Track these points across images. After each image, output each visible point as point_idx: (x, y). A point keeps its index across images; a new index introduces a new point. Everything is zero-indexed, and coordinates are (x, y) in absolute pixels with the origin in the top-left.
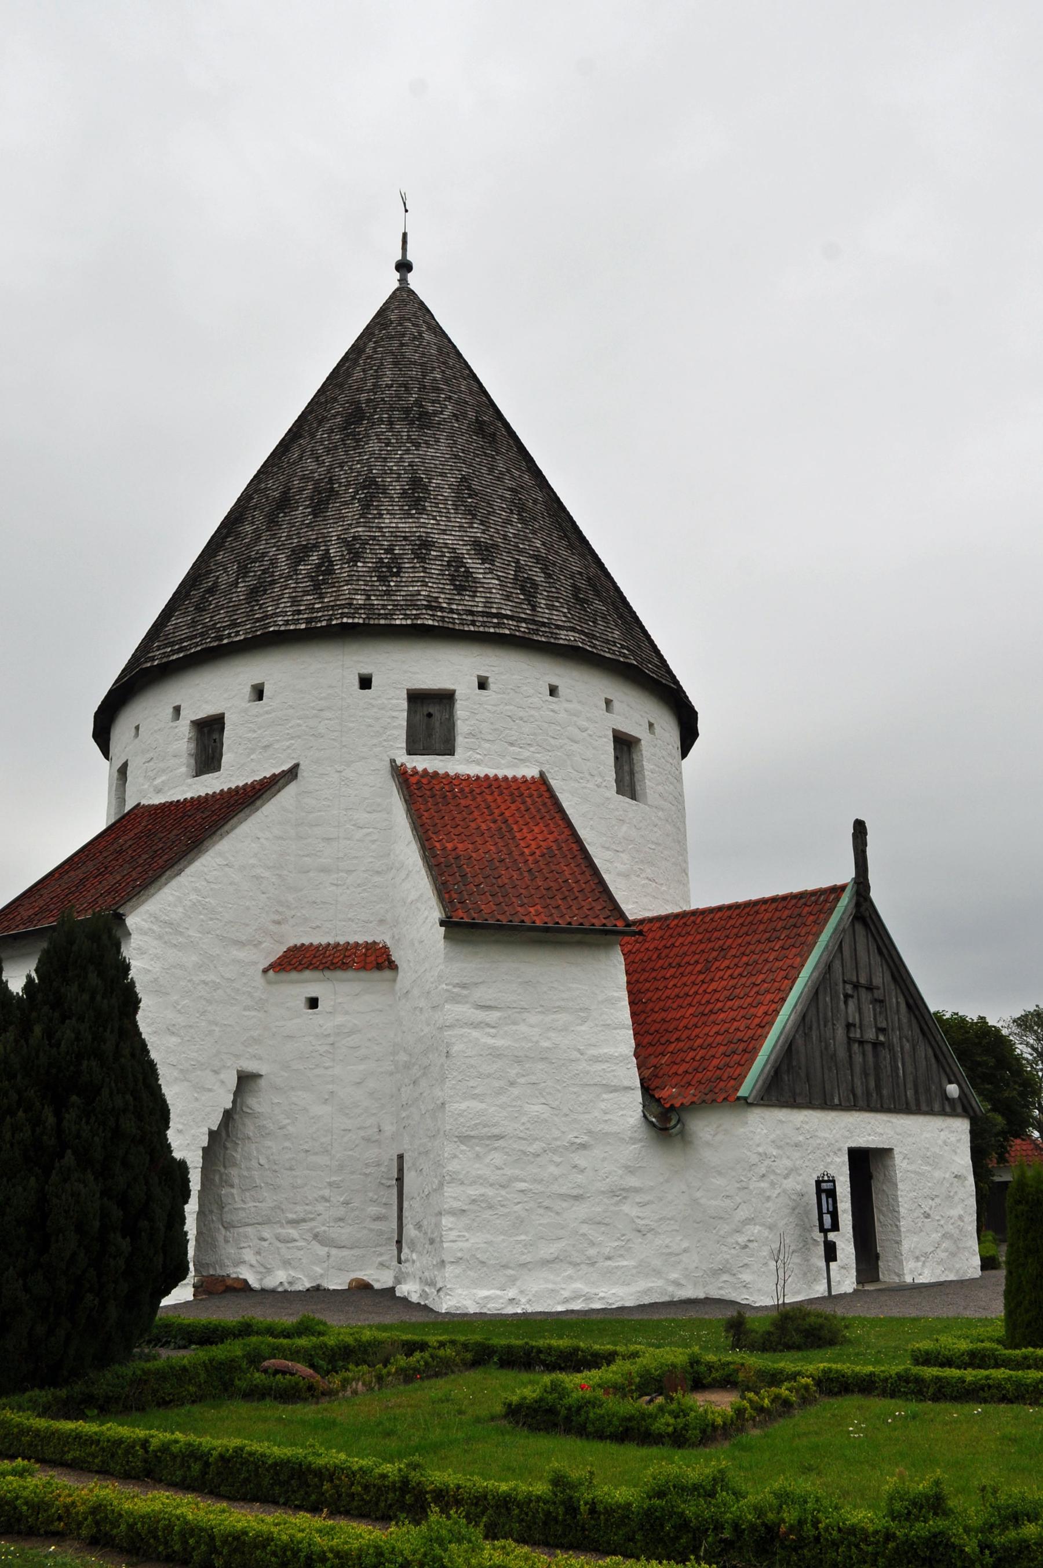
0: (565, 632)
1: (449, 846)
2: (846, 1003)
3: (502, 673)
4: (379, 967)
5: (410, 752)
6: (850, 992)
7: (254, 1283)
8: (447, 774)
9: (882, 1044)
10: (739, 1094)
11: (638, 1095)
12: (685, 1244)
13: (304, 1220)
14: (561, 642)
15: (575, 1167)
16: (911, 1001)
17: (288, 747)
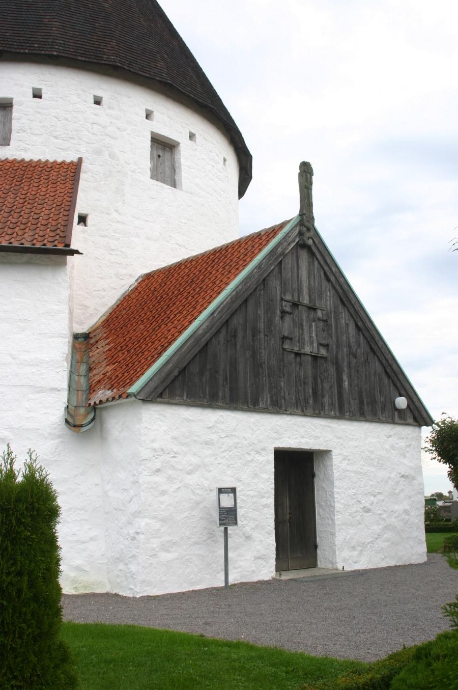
6: (288, 309)
16: (360, 324)
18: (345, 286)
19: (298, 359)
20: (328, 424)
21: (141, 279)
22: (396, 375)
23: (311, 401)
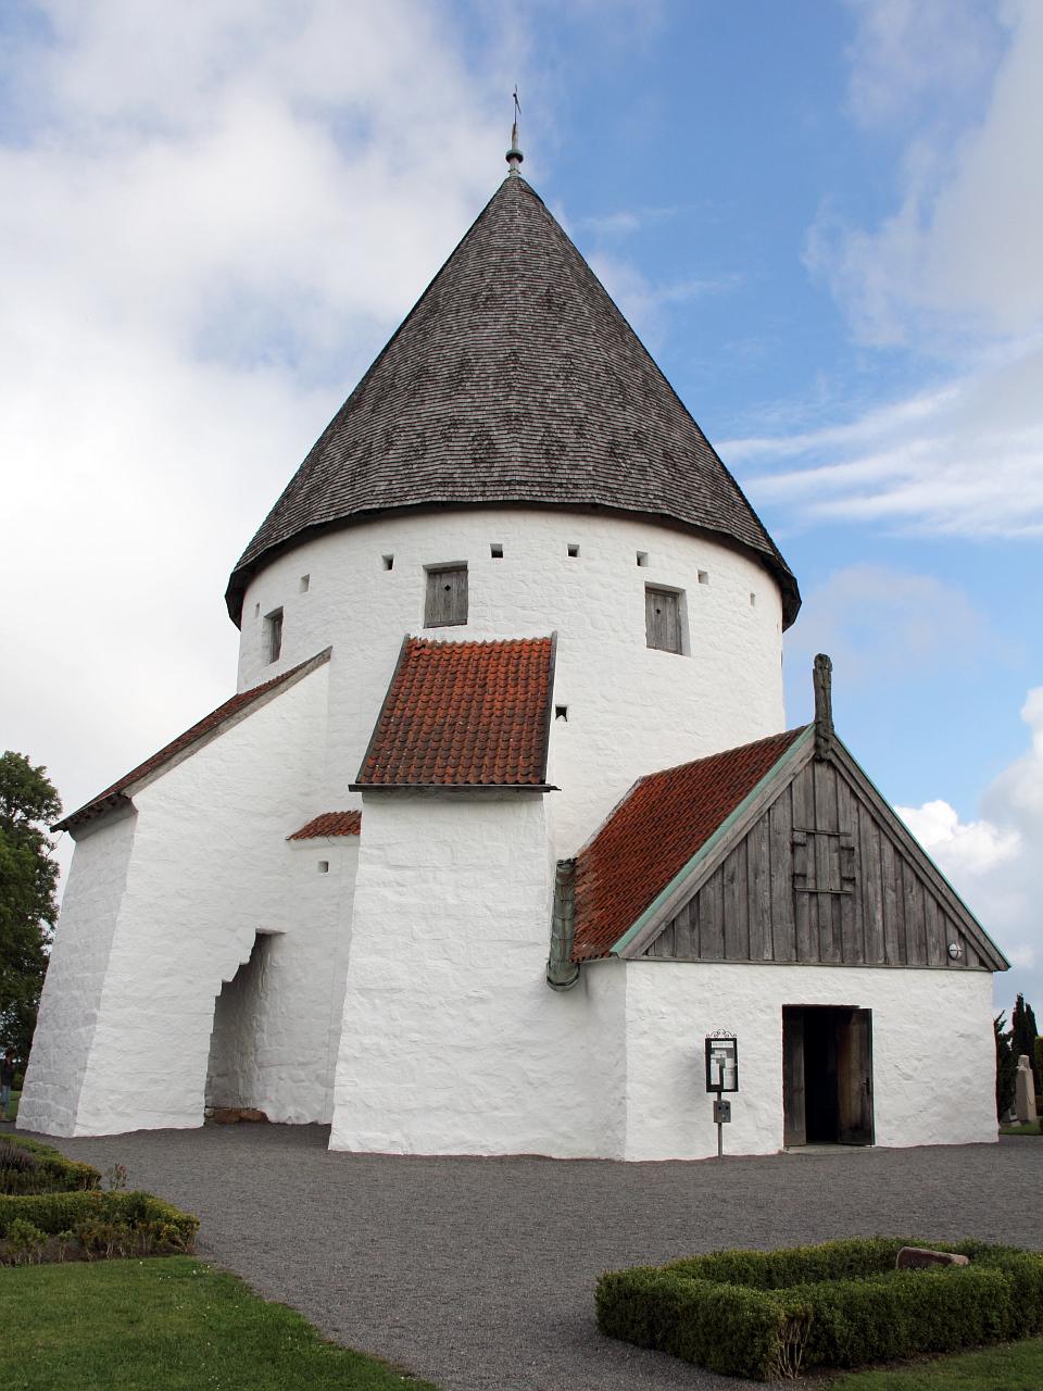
5: (428, 625)
7: (272, 1116)
15: (471, 1020)
16: (900, 848)
19: (814, 900)
20: (854, 974)
21: (639, 784)
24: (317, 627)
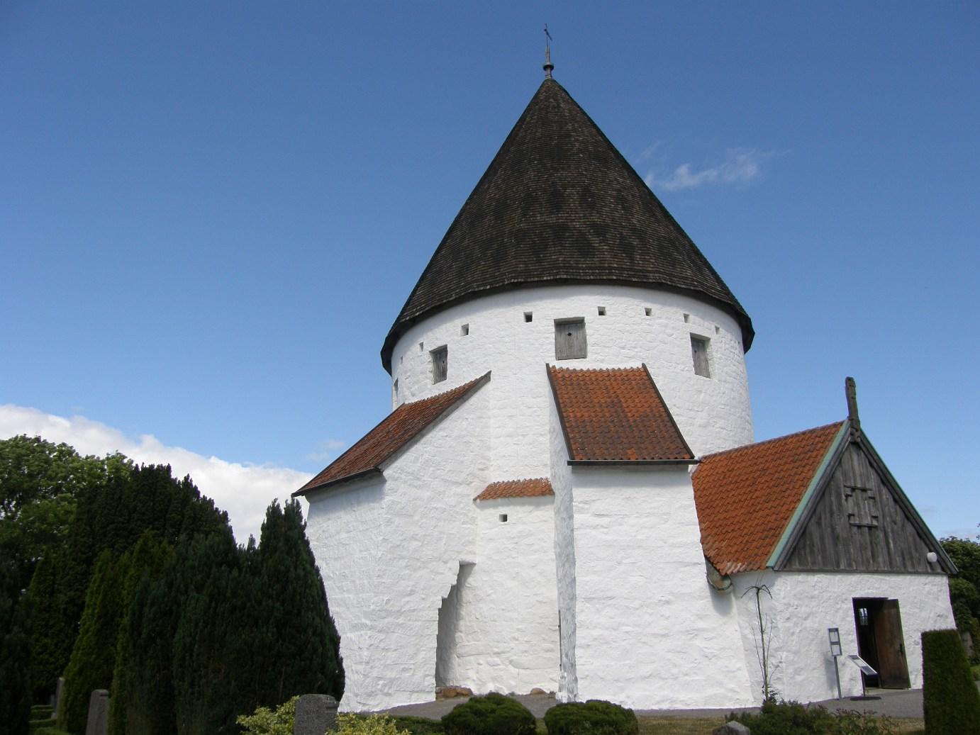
0: (653, 274)
1: (579, 415)
2: (846, 500)
3: (613, 304)
4: (543, 494)
5: (559, 358)
6: (849, 493)
8: (582, 370)
9: (876, 527)
10: (767, 565)
11: (703, 568)
12: (738, 665)
13: (503, 652)
14: (651, 281)
16: (896, 497)
17: (484, 362)
18: (884, 470)
22: (926, 536)
23: (871, 562)
24: (478, 359)
